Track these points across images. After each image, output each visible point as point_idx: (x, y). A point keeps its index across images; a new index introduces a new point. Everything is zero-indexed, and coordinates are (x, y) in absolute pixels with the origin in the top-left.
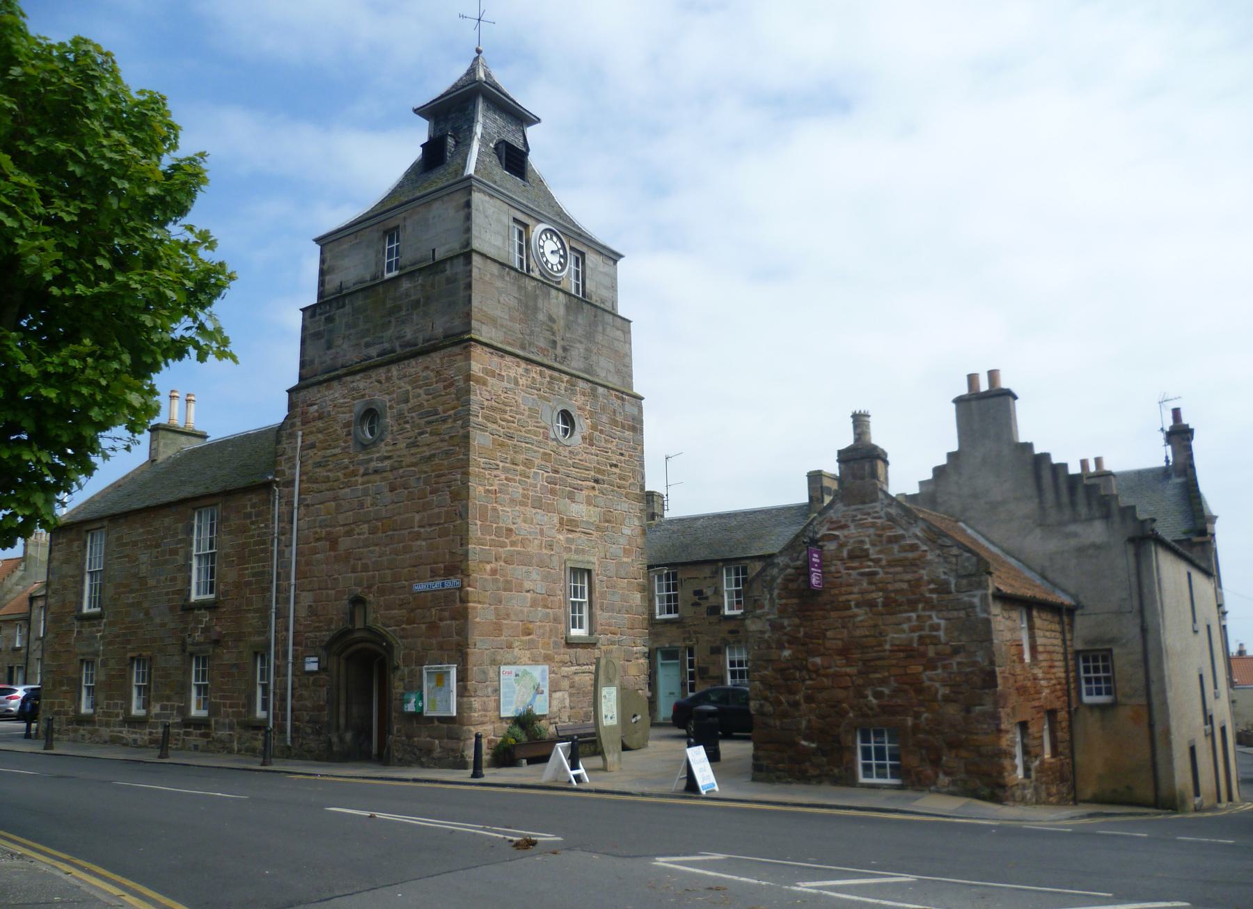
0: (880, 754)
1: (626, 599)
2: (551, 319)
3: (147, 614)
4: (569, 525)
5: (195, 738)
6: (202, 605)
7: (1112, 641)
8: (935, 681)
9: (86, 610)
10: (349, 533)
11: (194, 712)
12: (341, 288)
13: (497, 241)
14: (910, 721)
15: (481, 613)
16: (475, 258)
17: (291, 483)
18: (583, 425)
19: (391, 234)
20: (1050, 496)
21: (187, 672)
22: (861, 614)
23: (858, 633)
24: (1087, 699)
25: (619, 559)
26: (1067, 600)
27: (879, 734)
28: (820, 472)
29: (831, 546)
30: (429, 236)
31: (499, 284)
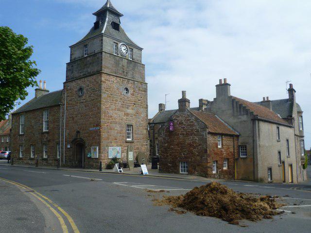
0: (184, 167)
1: (142, 132)
2: (123, 66)
3: (34, 134)
4: (127, 115)
5: (44, 163)
6: (46, 132)
7: (247, 143)
8: (195, 151)
9: (20, 133)
10: (76, 117)
11: (44, 157)
12: (75, 59)
13: (109, 48)
14: (190, 160)
15: (104, 135)
16: (103, 53)
17: (64, 105)
18: (131, 91)
19: (86, 46)
20: (235, 109)
21: (43, 148)
22: (181, 136)
23: (181, 140)
24: (241, 156)
25: (145, 124)
26: (237, 133)
27: (184, 163)
28: (202, 99)
29: (176, 121)
30: (93, 47)
31: (110, 59)
